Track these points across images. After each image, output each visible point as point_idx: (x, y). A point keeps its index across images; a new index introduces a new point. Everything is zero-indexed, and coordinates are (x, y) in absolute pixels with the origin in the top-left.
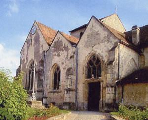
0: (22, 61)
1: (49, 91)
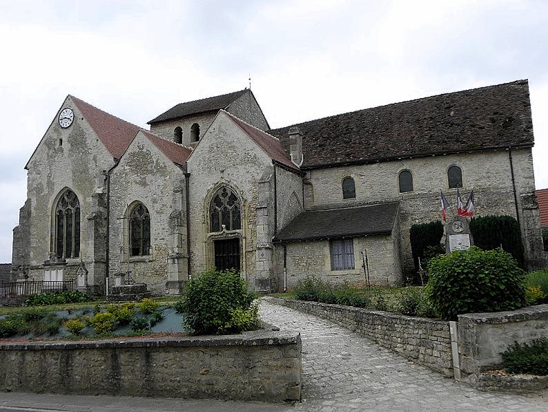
0: (33, 189)
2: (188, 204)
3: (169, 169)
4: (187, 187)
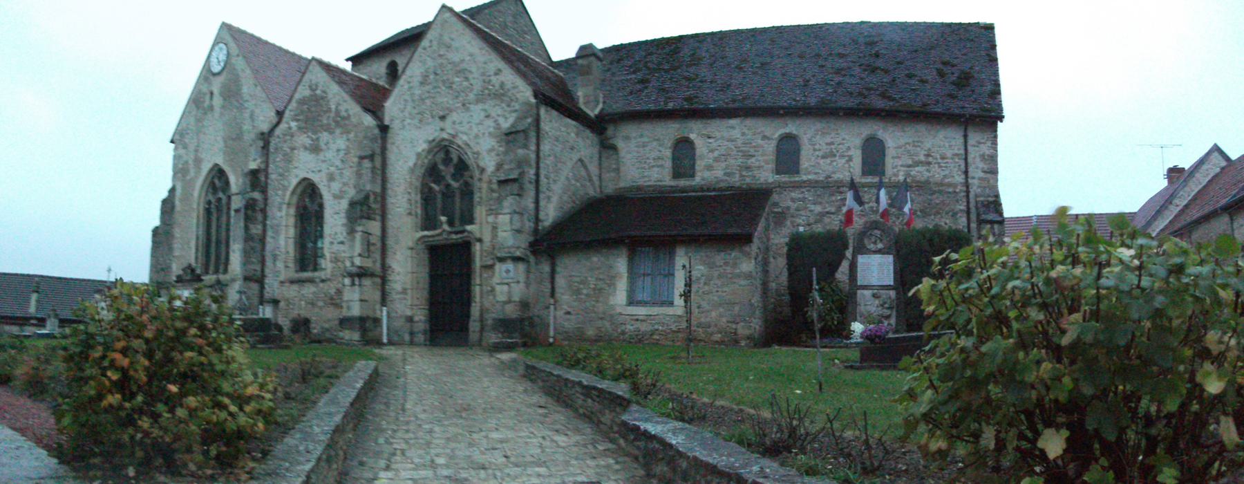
0: (180, 171)
1: (282, 278)
2: (384, 180)
3: (354, 120)
4: (384, 149)
